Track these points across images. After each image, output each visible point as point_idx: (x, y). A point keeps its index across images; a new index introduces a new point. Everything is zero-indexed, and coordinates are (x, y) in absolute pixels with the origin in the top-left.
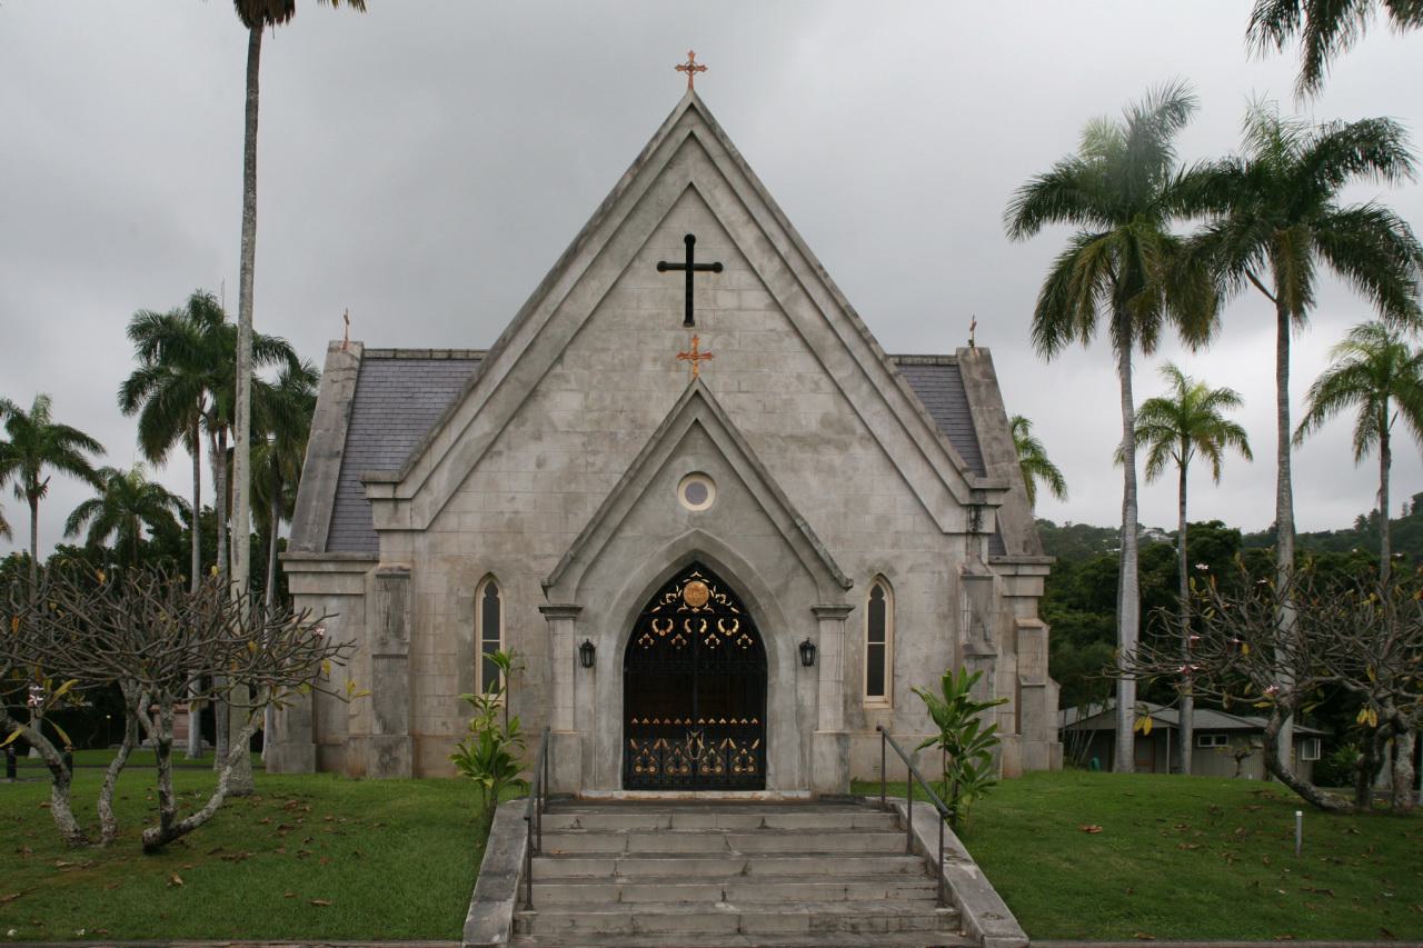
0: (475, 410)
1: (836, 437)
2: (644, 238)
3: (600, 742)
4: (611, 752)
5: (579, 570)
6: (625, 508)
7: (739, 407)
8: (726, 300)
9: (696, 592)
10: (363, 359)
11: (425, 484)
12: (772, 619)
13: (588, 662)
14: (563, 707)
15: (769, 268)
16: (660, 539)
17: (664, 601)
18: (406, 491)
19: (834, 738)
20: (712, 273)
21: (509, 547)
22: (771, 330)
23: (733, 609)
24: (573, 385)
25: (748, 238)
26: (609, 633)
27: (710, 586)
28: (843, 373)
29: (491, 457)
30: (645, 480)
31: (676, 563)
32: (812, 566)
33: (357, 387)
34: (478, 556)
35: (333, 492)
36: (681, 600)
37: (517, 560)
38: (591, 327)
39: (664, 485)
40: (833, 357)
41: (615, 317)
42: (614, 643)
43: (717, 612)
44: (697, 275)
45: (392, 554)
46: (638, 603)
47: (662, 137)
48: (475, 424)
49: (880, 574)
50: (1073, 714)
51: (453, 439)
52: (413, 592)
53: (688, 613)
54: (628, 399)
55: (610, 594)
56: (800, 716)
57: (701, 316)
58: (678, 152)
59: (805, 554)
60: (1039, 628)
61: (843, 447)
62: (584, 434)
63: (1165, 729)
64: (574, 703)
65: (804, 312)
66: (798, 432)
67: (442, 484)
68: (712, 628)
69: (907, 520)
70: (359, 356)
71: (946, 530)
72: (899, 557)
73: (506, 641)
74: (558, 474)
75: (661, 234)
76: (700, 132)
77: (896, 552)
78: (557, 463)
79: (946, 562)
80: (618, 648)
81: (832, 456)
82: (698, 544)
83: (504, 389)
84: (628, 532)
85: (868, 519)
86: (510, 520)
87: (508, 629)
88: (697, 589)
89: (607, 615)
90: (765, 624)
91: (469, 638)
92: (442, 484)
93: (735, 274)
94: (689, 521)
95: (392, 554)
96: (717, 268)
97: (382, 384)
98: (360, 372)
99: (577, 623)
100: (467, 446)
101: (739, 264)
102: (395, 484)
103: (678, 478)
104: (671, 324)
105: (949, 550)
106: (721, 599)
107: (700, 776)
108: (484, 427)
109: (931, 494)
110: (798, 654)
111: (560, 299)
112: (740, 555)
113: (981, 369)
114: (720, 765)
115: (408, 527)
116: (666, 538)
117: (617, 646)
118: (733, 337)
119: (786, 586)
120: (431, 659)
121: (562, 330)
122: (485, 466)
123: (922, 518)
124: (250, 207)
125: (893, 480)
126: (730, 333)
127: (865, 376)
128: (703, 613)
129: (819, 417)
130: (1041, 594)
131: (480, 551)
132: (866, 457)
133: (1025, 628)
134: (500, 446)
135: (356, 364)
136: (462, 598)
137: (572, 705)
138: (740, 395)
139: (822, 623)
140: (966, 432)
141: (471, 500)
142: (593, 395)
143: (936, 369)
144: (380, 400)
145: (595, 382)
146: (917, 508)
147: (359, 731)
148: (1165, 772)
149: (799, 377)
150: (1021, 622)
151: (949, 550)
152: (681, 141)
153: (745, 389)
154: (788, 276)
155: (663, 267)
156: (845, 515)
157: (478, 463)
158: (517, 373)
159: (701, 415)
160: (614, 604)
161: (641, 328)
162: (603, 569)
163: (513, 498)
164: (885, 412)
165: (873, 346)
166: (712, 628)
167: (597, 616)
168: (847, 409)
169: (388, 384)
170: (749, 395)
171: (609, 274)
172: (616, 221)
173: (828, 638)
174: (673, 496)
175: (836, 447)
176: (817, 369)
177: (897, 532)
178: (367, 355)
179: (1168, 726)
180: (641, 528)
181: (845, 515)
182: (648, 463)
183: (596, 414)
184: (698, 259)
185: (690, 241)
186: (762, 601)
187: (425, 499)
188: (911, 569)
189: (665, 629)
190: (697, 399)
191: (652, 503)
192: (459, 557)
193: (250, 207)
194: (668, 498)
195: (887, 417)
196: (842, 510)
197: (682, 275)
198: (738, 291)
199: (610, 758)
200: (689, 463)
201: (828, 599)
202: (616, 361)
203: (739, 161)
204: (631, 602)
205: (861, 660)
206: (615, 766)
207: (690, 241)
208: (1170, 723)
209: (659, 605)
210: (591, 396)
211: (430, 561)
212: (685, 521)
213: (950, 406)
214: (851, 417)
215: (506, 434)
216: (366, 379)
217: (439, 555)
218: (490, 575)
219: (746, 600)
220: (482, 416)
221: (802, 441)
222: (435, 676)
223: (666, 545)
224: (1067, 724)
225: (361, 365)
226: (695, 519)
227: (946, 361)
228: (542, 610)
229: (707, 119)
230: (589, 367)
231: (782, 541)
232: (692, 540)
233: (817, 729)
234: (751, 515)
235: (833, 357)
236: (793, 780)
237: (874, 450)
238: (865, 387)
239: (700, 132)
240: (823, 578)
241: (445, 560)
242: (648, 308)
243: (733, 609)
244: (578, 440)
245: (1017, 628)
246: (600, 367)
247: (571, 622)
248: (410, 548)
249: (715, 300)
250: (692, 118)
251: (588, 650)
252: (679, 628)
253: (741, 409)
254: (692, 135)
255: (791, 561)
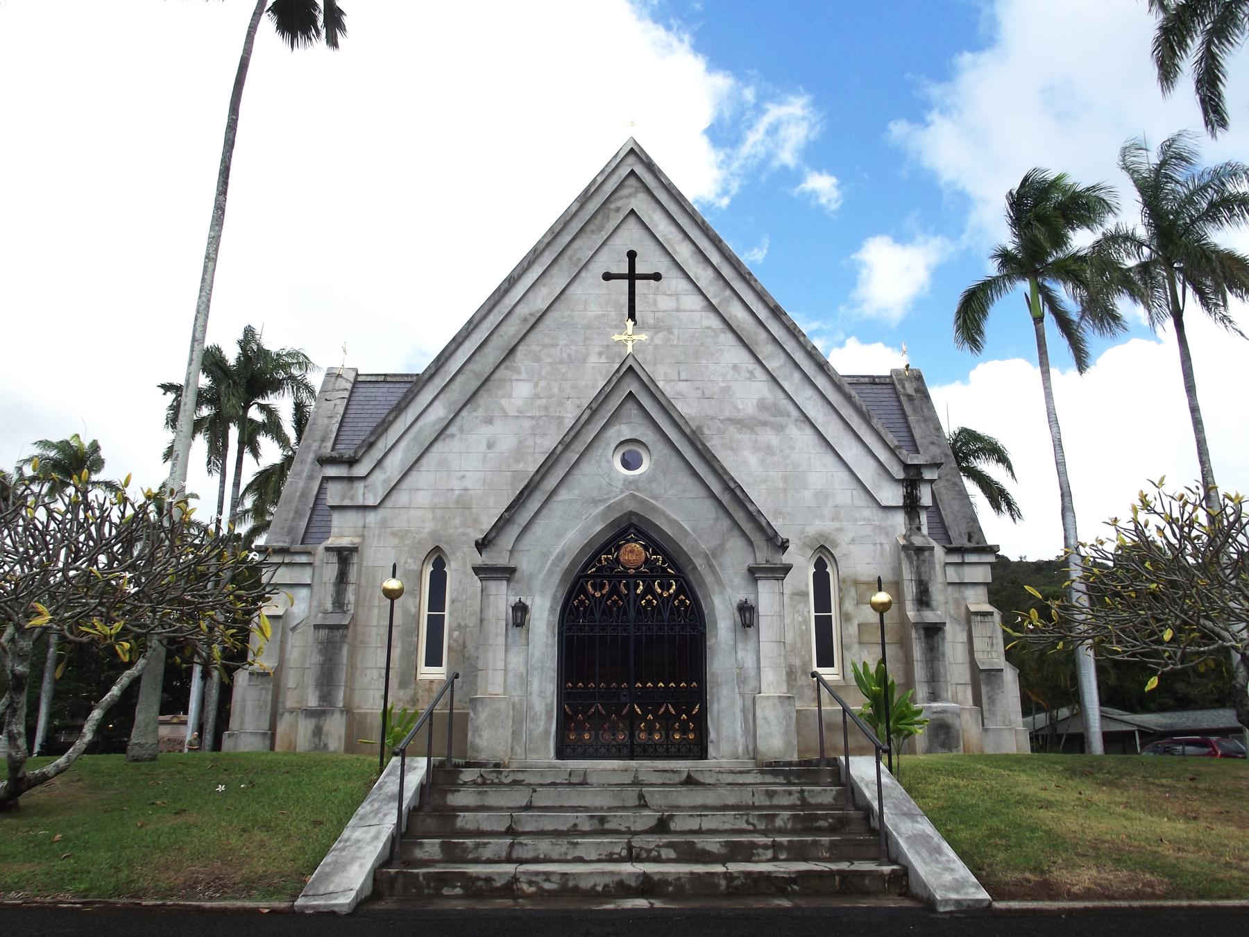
0: (431, 398)
1: (772, 419)
2: (591, 253)
3: (530, 707)
4: (543, 717)
5: (513, 531)
6: (559, 472)
7: (678, 394)
8: (665, 303)
9: (633, 553)
10: (356, 382)
11: (379, 463)
12: (709, 579)
13: (519, 621)
14: (494, 670)
15: (704, 277)
16: (595, 502)
17: (600, 561)
18: (361, 470)
19: (776, 701)
20: (652, 281)
21: (457, 521)
22: (707, 328)
23: (669, 570)
24: (524, 376)
25: (683, 252)
26: (543, 593)
27: (646, 548)
28: (776, 363)
29: (444, 439)
30: (579, 446)
31: (612, 525)
32: (747, 527)
33: (346, 409)
34: (427, 530)
35: (315, 492)
36: (617, 560)
37: (464, 534)
38: (541, 327)
39: (599, 452)
40: (765, 349)
41: (563, 318)
42: (548, 604)
43: (651, 572)
44: (639, 283)
45: (342, 532)
46: (573, 563)
47: (606, 173)
48: (430, 410)
49: (822, 546)
50: (1041, 719)
51: (409, 423)
52: (360, 565)
53: (624, 575)
54: (574, 387)
55: (545, 555)
56: (741, 679)
57: (642, 317)
58: (620, 186)
59: (739, 516)
60: (991, 614)
61: (779, 428)
62: (532, 418)
63: (1133, 733)
64: (506, 666)
65: (736, 312)
66: (736, 415)
67: (395, 463)
68: (649, 590)
69: (845, 494)
70: (352, 380)
71: (884, 503)
72: (840, 530)
73: (451, 614)
74: (506, 454)
75: (606, 249)
76: (639, 170)
77: (837, 525)
78: (506, 444)
79: (887, 534)
80: (552, 610)
81: (769, 437)
82: (633, 507)
83: (459, 379)
84: (563, 495)
85: (808, 494)
86: (459, 496)
87: (453, 602)
88: (632, 551)
89: (542, 576)
90: (702, 583)
91: (413, 610)
92: (395, 463)
93: (673, 282)
94: (624, 485)
95: (342, 532)
96: (657, 277)
97: (371, 403)
98: (352, 392)
99: (512, 585)
100: (421, 430)
101: (675, 273)
102: (352, 462)
103: (613, 446)
104: (615, 323)
105: (889, 522)
106: (657, 560)
107: (639, 745)
108: (439, 412)
109: (866, 470)
110: (737, 614)
111: (514, 303)
112: (674, 516)
113: (915, 385)
114: (659, 730)
115: (360, 503)
116: (600, 501)
117: (551, 607)
118: (672, 333)
119: (722, 546)
120: (374, 630)
121: (512, 329)
122: (438, 447)
123: (859, 493)
124: (220, 209)
125: (829, 459)
126: (669, 330)
127: (797, 365)
128: (639, 575)
129: (755, 402)
130: (990, 580)
131: (429, 526)
132: (804, 437)
133: (977, 613)
134: (453, 429)
135: (349, 386)
136: (409, 571)
137: (503, 667)
138: (680, 383)
139: (760, 583)
140: (894, 399)
141: (421, 478)
142: (542, 384)
143: (874, 387)
144: (368, 415)
145: (544, 372)
146: (854, 485)
147: (295, 705)
148: (1135, 752)
149: (735, 367)
150: (973, 608)
151: (889, 522)
152: (623, 176)
153: (685, 378)
154: (721, 282)
155: (607, 277)
156: (785, 490)
157: (431, 444)
158: (469, 367)
159: (634, 387)
160: (548, 565)
161: (588, 327)
162: (538, 530)
163: (463, 477)
164: (817, 397)
165: (801, 339)
166: (649, 590)
167: (531, 577)
168: (781, 395)
169: (377, 403)
170: (688, 383)
171: (558, 281)
172: (565, 239)
173: (766, 597)
174: (609, 462)
175: (772, 428)
176: (752, 360)
177: (836, 506)
178: (360, 379)
179: (1136, 728)
180: (577, 492)
181: (785, 490)
182: (584, 431)
183: (544, 401)
184: (639, 270)
185: (632, 255)
186: (699, 562)
187: (378, 476)
188: (853, 541)
189: (601, 590)
190: (630, 374)
191: (587, 467)
192: (408, 531)
193: (220, 209)
194: (604, 464)
195: (820, 402)
196: (781, 485)
197: (625, 284)
198: (677, 296)
199: (542, 724)
200: (623, 430)
201: (763, 555)
202: (564, 355)
203: (673, 192)
204: (566, 563)
205: (808, 630)
206: (547, 732)
207: (632, 255)
208: (1138, 726)
209: (595, 565)
210: (540, 384)
211: (379, 536)
212: (620, 485)
213: (889, 417)
214: (784, 403)
215: (459, 420)
216: (357, 397)
217: (389, 530)
218: (437, 549)
219: (681, 561)
220: (437, 403)
221: (742, 424)
222: (377, 648)
223: (602, 507)
224: (1036, 728)
225: (353, 387)
226: (630, 482)
227: (882, 381)
228: (477, 570)
229: (644, 159)
230: (537, 359)
231: (715, 503)
232: (626, 503)
233: (760, 693)
234: (686, 480)
235: (765, 349)
236: (736, 748)
237: (808, 431)
238: (797, 376)
239: (639, 170)
240: (757, 538)
241: (394, 534)
242: (594, 310)
243: (669, 570)
244: (527, 424)
245: (970, 614)
246: (549, 360)
247: (505, 583)
248: (361, 523)
249: (655, 302)
250: (631, 159)
251: (520, 613)
252: (615, 590)
253: (682, 396)
254: (632, 173)
255: (725, 523)
